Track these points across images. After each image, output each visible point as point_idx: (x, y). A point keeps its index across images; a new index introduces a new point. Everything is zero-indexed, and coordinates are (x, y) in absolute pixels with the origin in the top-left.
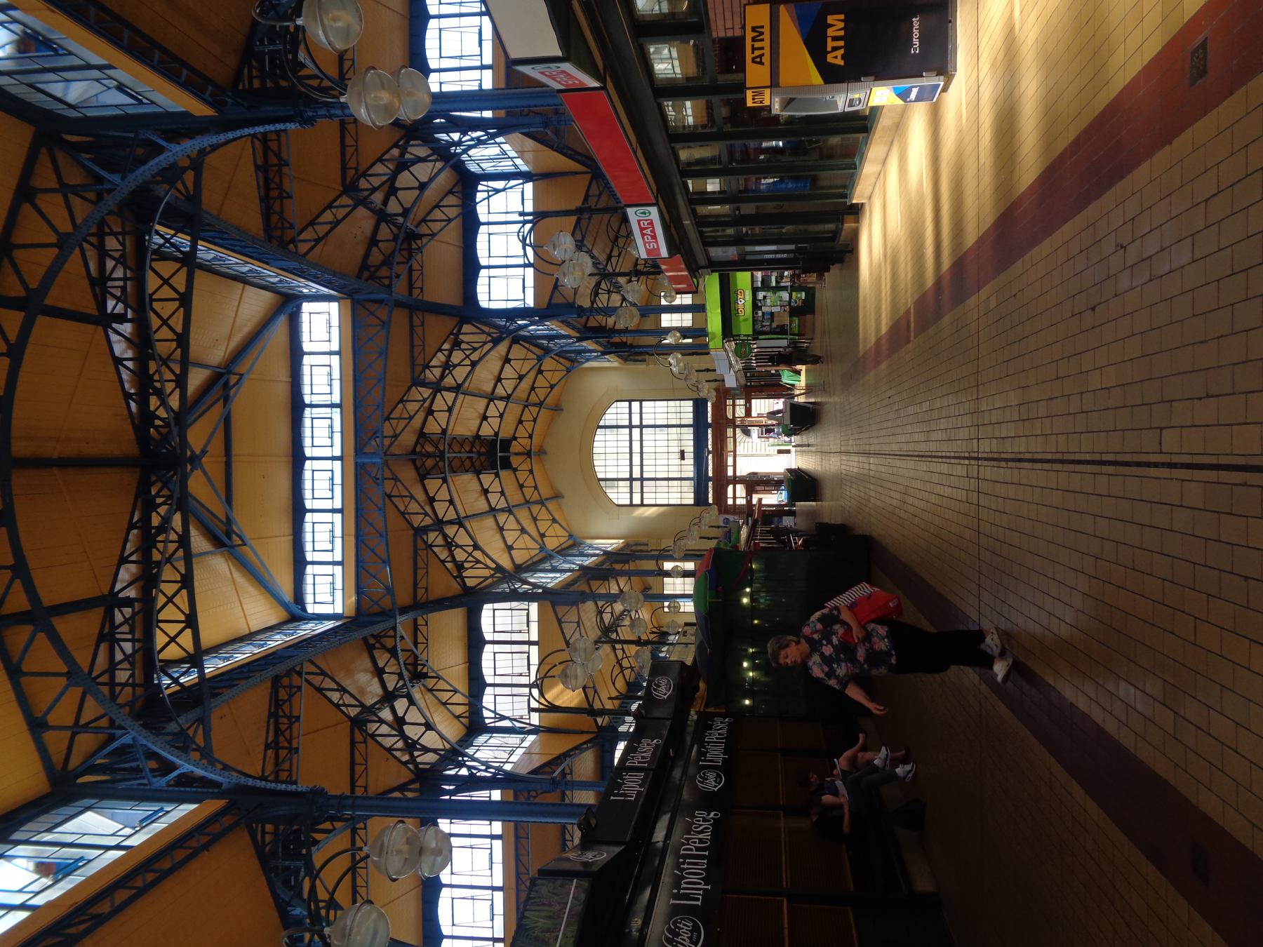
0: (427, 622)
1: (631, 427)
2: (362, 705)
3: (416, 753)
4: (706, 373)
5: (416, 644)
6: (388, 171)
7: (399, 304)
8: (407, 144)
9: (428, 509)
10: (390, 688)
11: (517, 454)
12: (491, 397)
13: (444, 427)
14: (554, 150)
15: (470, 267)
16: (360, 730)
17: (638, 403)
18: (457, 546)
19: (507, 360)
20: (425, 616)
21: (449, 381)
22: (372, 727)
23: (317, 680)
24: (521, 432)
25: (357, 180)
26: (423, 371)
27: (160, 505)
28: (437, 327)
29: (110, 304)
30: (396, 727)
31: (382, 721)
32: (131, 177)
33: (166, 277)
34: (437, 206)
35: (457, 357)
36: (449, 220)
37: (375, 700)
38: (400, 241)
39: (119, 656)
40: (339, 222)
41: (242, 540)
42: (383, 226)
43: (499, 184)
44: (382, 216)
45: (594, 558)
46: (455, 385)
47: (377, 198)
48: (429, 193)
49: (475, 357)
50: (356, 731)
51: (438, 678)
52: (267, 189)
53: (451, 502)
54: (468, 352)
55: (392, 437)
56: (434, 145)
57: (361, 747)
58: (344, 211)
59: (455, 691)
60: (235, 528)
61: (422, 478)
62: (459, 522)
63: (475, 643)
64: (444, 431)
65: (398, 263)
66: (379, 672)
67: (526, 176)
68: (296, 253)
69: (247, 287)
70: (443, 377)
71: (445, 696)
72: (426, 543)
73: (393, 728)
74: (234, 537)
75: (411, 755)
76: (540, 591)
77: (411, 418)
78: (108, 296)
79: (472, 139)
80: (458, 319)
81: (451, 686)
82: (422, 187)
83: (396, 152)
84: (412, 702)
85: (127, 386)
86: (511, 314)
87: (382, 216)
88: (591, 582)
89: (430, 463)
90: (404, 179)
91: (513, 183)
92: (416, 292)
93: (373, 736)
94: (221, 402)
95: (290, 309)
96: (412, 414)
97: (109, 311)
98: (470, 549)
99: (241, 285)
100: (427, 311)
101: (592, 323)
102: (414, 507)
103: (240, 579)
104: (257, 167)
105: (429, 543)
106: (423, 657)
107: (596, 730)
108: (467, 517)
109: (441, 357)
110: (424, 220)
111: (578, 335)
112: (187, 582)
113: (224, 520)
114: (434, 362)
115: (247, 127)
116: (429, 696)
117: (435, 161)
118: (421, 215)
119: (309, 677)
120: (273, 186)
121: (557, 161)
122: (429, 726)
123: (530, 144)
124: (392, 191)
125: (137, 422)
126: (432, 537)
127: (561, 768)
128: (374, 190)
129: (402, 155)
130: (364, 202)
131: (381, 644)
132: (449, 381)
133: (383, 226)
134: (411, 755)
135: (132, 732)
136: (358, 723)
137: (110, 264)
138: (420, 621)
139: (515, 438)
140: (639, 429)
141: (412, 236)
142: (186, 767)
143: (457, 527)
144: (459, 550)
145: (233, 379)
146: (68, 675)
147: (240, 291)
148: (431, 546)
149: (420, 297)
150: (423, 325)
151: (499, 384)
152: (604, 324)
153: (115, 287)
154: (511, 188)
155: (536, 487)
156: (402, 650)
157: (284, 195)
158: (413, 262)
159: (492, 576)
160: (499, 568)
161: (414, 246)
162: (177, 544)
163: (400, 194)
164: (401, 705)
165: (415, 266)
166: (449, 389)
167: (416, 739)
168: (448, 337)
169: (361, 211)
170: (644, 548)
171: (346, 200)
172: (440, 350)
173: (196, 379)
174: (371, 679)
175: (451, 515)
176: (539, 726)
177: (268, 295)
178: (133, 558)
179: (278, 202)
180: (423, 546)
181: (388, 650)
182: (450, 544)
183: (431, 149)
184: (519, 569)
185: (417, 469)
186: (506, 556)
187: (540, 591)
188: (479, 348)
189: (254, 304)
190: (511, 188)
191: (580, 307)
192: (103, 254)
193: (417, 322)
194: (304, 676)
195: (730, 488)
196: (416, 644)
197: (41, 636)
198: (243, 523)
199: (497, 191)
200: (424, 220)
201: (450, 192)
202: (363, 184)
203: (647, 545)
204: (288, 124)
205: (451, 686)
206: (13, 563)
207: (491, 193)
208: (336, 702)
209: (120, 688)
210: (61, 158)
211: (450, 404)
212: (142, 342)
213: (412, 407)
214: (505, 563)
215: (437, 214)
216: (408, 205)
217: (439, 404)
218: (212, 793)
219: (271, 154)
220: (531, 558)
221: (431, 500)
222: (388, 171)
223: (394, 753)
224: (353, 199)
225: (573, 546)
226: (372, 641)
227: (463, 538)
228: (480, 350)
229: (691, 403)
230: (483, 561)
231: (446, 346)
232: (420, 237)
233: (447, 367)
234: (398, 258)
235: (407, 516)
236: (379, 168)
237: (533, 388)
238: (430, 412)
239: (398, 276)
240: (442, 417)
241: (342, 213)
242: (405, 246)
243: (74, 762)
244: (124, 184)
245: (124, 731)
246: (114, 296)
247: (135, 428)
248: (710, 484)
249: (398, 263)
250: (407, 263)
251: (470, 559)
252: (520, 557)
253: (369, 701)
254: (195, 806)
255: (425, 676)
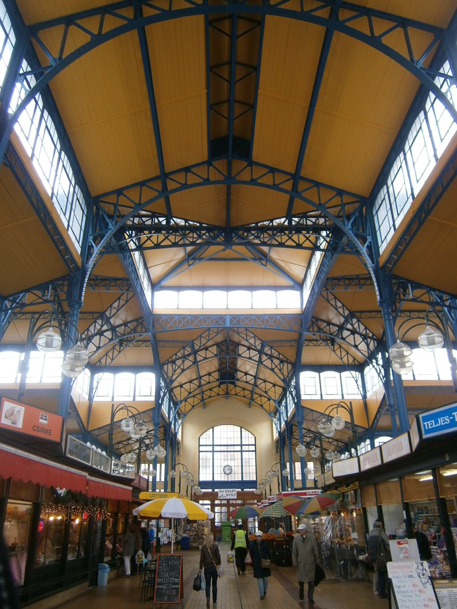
0: (147, 346)
1: (241, 445)
2: (110, 318)
3: (85, 341)
4: (269, 489)
5: (137, 341)
6: (361, 332)
7: (300, 335)
8: (374, 340)
9: (203, 347)
10: (117, 329)
11: (227, 387)
12: (257, 377)
13: (242, 355)
14: (378, 409)
15: (319, 368)
16: (99, 317)
17: (254, 449)
18: (183, 362)
19: (274, 385)
20: (151, 345)
21: (264, 358)
22: (100, 322)
23: (124, 297)
24: (238, 390)
25: (356, 318)
26: (269, 346)
27: (209, 234)
28: (291, 354)
29: (296, 219)
30: (99, 332)
31: (102, 326)
32: (351, 232)
33: (307, 241)
34: (347, 353)
35: (277, 362)
36: (341, 359)
37: (112, 323)
38: (330, 336)
39: (144, 219)
40: (337, 309)
41: (191, 265)
42: (337, 328)
43: (360, 382)
44: (341, 328)
45: (167, 415)
46: (262, 361)
47: (349, 326)
48: (354, 349)
49: (276, 370)
50: (98, 315)
51: (120, 352)
52: (349, 279)
53: (205, 358)
54: (279, 367)
55: (238, 332)
56: (375, 351)
57: (91, 317)
58: (342, 312)
59: (112, 360)
60: (197, 262)
61: (217, 345)
62: (195, 362)
63: (136, 368)
64: (240, 355)
65: (320, 335)
66: (125, 324)
67: (365, 397)
68: (322, 291)
69: (306, 268)
70: (266, 355)
71: (110, 354)
72: (186, 346)
73: (99, 330)
74: (192, 261)
75: (85, 339)
76: (160, 402)
77: (247, 340)
78: (300, 219)
79: (380, 370)
80: (294, 362)
81: (115, 358)
82: (356, 346)
83: (371, 335)
84: (111, 340)
85: (262, 223)
86: (297, 388)
87: (341, 328)
88: (163, 428)
89: (224, 348)
90: (358, 339)
91: (361, 389)
92: (306, 343)
93: (95, 322)
94: (253, 257)
95: (296, 286)
96: (249, 341)
97: (293, 219)
98: (182, 367)
99: (306, 266)
100: (298, 348)
101: (294, 428)
102: (204, 341)
103: (173, 263)
104: (358, 275)
105: (186, 348)
106: (131, 345)
107: (89, 430)
108: (198, 365)
109: (276, 354)
110: (340, 347)
111: (288, 421)
112: (175, 245)
113: (201, 257)
114: (273, 351)
115: (376, 279)
116: (111, 347)
117: (368, 352)
118: (343, 346)
119: (126, 294)
120: (351, 281)
121: (373, 410)
122: (98, 348)
123: (380, 398)
124: (353, 332)
125: (246, 227)
126: (188, 350)
127: (72, 412)
128: (352, 325)
129: (369, 338)
130: (347, 320)
131: (139, 324)
132: (264, 358)
133: (337, 328)
134: (85, 339)
135: (113, 228)
136: (102, 315)
137: (314, 220)
138: (148, 343)
139: (235, 386)
140: (240, 450)
141: (333, 342)
142: (96, 250)
143: (193, 361)
144: (182, 362)
145: (263, 262)
146: (140, 204)
147: (303, 265)
148: (184, 348)
149: (304, 345)
150: (291, 346)
151: (263, 381)
152: (295, 434)
153: (303, 221)
154: (358, 388)
155: (210, 397)
156: (134, 336)
157: (347, 286)
158: (321, 341)
159: (168, 377)
160: (172, 381)
161: (329, 342)
162: (169, 177)
163: (352, 336)
164: (108, 334)
165: (319, 343)
166: (260, 358)
167: (92, 341)
168: (286, 357)
169: (342, 320)
170: (177, 454)
171: (347, 313)
172: (279, 354)
173: (265, 249)
174: (122, 321)
175: (199, 358)
176: (92, 401)
177: (302, 276)
178: (187, 224)
179: (343, 283)
180: (185, 345)
181: (134, 329)
182: (185, 357)
183: (374, 351)
184: (171, 391)
185: (221, 342)
186: (178, 384)
187: (160, 402)
188: (281, 372)
189: (298, 271)
190: (358, 388)
191: (302, 423)
192: (317, 217)
193: (292, 343)
194: (126, 292)
195: (209, 502)
196: (137, 341)
197: (157, 194)
198: (199, 265)
199: (356, 381)
200: (340, 347)
201: (354, 359)
202: (354, 320)
203: (178, 454)
204: (379, 296)
205: (115, 358)
206: (188, 184)
207: (355, 378)
208: (113, 306)
209: (132, 220)
210: (357, 205)
211: (253, 358)
212: (281, 229)
213: (252, 341)
214: (176, 384)
215: (344, 353)
216: (347, 339)
217: (253, 353)
218: (84, 260)
219: (365, 281)
220: (175, 395)
221: (206, 349)
222: (361, 332)
223: (86, 332)
224: (348, 315)
225: (180, 415)
226: (140, 321)
227: (188, 363)
228: (280, 372)
229: (255, 479)
230: (176, 373)
231: (281, 356)
232: (333, 345)
233: (271, 357)
234: (323, 335)
235: (199, 337)
236: (362, 328)
237: (261, 396)
238: (249, 348)
239: (314, 335)
240: (246, 354)
241: (341, 310)
242: (328, 338)
243: (101, 204)
244: (348, 227)
245: (114, 225)
246: (300, 221)
247: (243, 226)
248: (211, 490)
249: (320, 335)
250: (320, 339)
251: (177, 367)
252: (177, 391)
253: (112, 321)
254: (80, 254)
255: (121, 345)
